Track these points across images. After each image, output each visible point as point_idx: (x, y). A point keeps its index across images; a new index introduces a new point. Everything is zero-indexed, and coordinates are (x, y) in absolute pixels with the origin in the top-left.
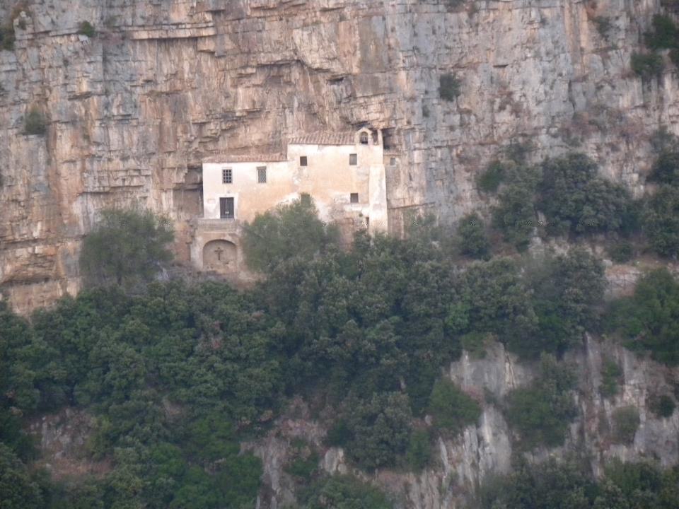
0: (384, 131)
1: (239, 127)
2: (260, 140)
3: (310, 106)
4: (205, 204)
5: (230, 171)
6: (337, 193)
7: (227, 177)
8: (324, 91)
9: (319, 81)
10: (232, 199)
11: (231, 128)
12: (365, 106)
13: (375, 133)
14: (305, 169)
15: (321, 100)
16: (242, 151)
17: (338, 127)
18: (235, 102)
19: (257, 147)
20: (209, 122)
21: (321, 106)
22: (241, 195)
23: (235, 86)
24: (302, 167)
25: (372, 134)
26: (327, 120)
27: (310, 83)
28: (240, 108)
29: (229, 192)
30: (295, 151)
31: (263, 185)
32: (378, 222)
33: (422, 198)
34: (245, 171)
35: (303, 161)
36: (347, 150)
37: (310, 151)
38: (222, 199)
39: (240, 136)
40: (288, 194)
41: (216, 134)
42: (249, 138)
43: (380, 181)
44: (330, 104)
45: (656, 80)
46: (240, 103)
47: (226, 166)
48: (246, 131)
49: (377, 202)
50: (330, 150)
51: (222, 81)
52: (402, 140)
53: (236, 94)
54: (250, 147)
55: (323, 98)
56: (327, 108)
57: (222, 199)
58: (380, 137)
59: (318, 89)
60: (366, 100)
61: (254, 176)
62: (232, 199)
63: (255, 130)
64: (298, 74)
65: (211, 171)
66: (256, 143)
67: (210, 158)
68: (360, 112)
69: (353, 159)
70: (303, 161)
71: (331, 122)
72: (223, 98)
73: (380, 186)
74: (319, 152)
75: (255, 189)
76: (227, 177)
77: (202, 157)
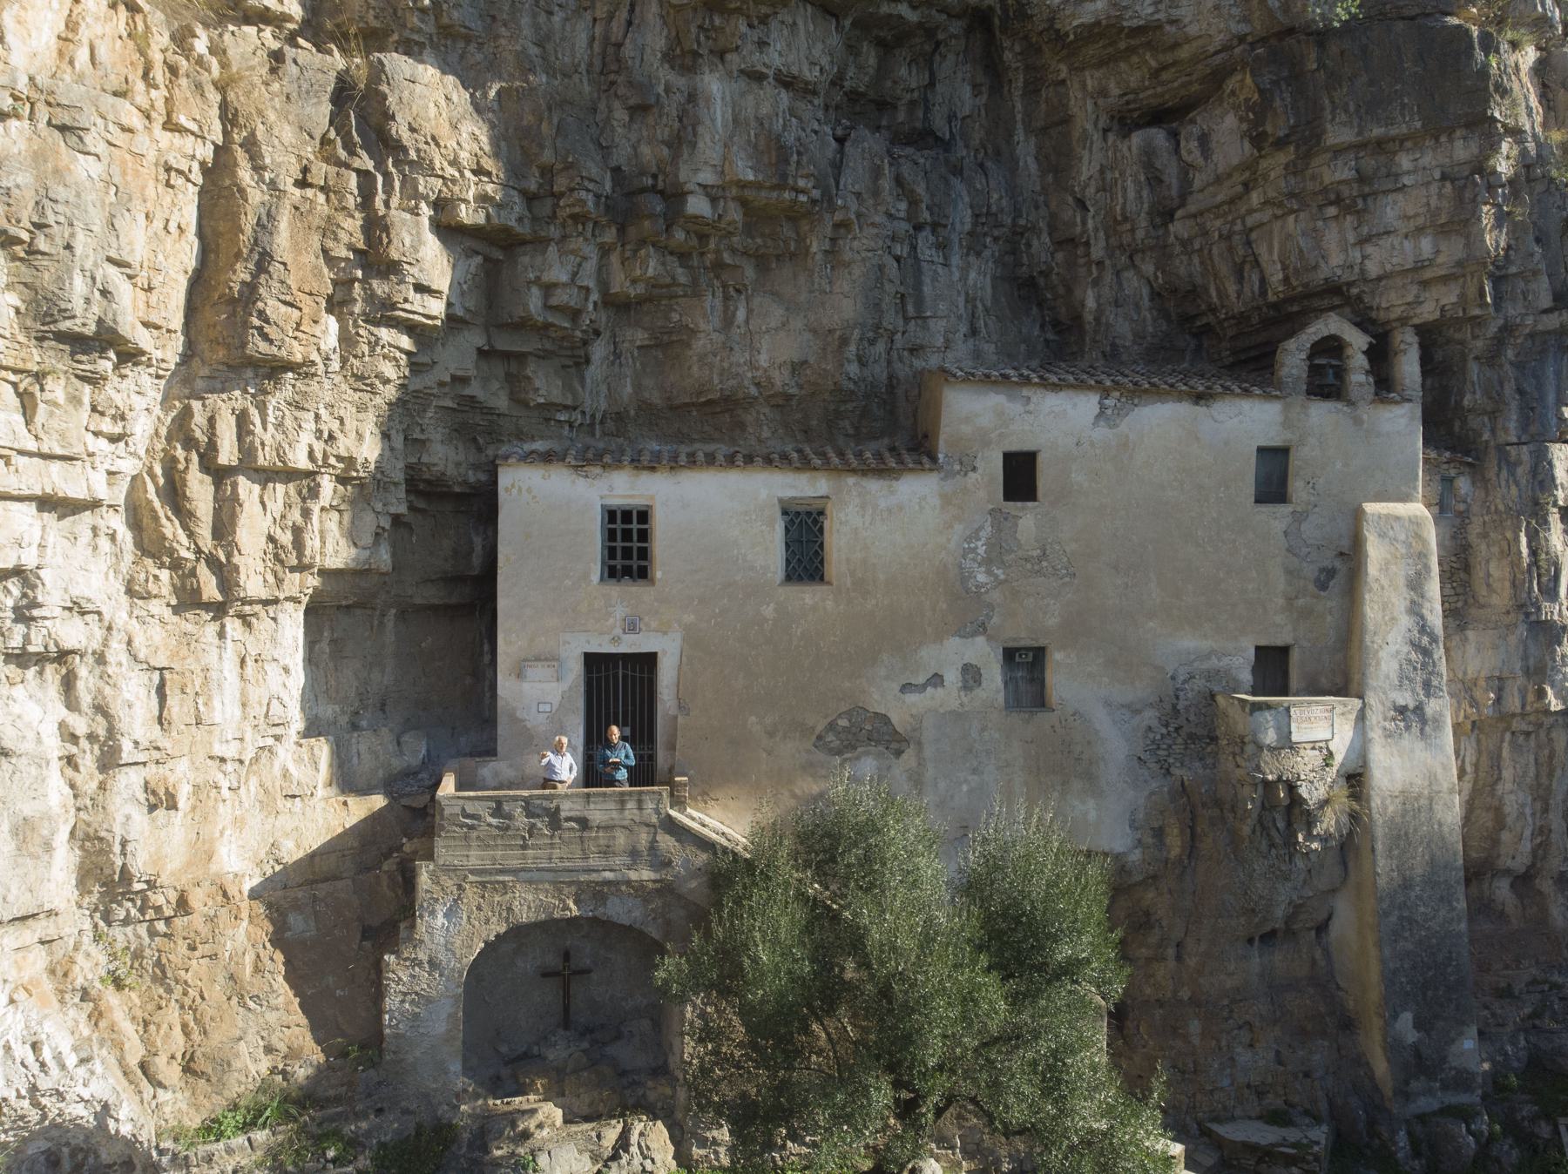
0: (1429, 336)
1: (695, 291)
2: (797, 367)
3: (1016, 239)
4: (506, 685)
5: (644, 516)
6: (1189, 642)
7: (628, 545)
8: (1087, 168)
9: (1067, 120)
10: (648, 662)
11: (657, 296)
12: (1354, 202)
13: (1380, 356)
14: (1027, 518)
15: (1069, 213)
16: (703, 427)
17: (1139, 336)
18: (682, 140)
19: (781, 403)
20: (540, 243)
21: (1068, 242)
22: (694, 641)
23: (683, 59)
24: (1013, 507)
25: (1370, 353)
26: (1091, 303)
27: (1020, 135)
28: (707, 177)
29: (632, 627)
30: (979, 416)
31: (808, 595)
32: (1414, 806)
33: (353, 551)
34: (717, 511)
35: (1020, 476)
36: (1249, 421)
37: (1060, 419)
38: (593, 662)
39: (700, 344)
40: (939, 638)
41: (575, 314)
42: (740, 357)
43: (1416, 584)
44: (1113, 225)
45: (436, 601)
46: (709, 147)
47: (625, 487)
48: (728, 321)
49: (1405, 698)
50: (1161, 421)
51: (617, 28)
52: (1509, 389)
53: (692, 98)
54: (750, 402)
55: (1081, 204)
56: (1097, 251)
57: (593, 662)
58: (1409, 367)
59: (1058, 163)
60: (1369, 163)
61: (769, 549)
62: (648, 662)
63: (777, 313)
64: (967, 91)
65: (548, 506)
66: (780, 379)
67: (539, 446)
68: (1316, 235)
69: (1274, 475)
70: (1020, 476)
71: (1110, 315)
72: (621, 115)
73: (1415, 610)
74: (1102, 433)
75: (768, 611)
76: (628, 545)
77: (494, 435)
